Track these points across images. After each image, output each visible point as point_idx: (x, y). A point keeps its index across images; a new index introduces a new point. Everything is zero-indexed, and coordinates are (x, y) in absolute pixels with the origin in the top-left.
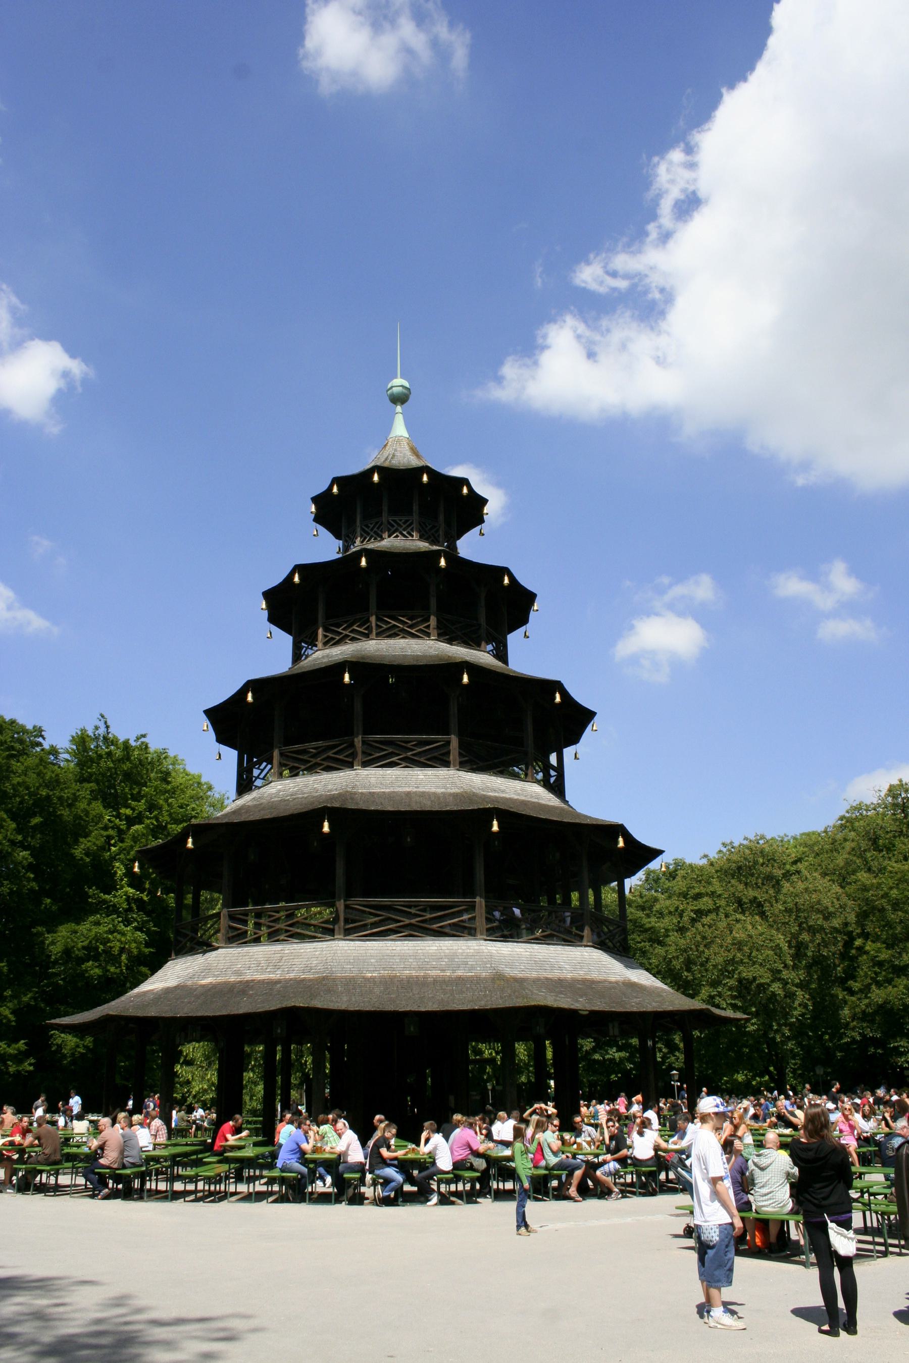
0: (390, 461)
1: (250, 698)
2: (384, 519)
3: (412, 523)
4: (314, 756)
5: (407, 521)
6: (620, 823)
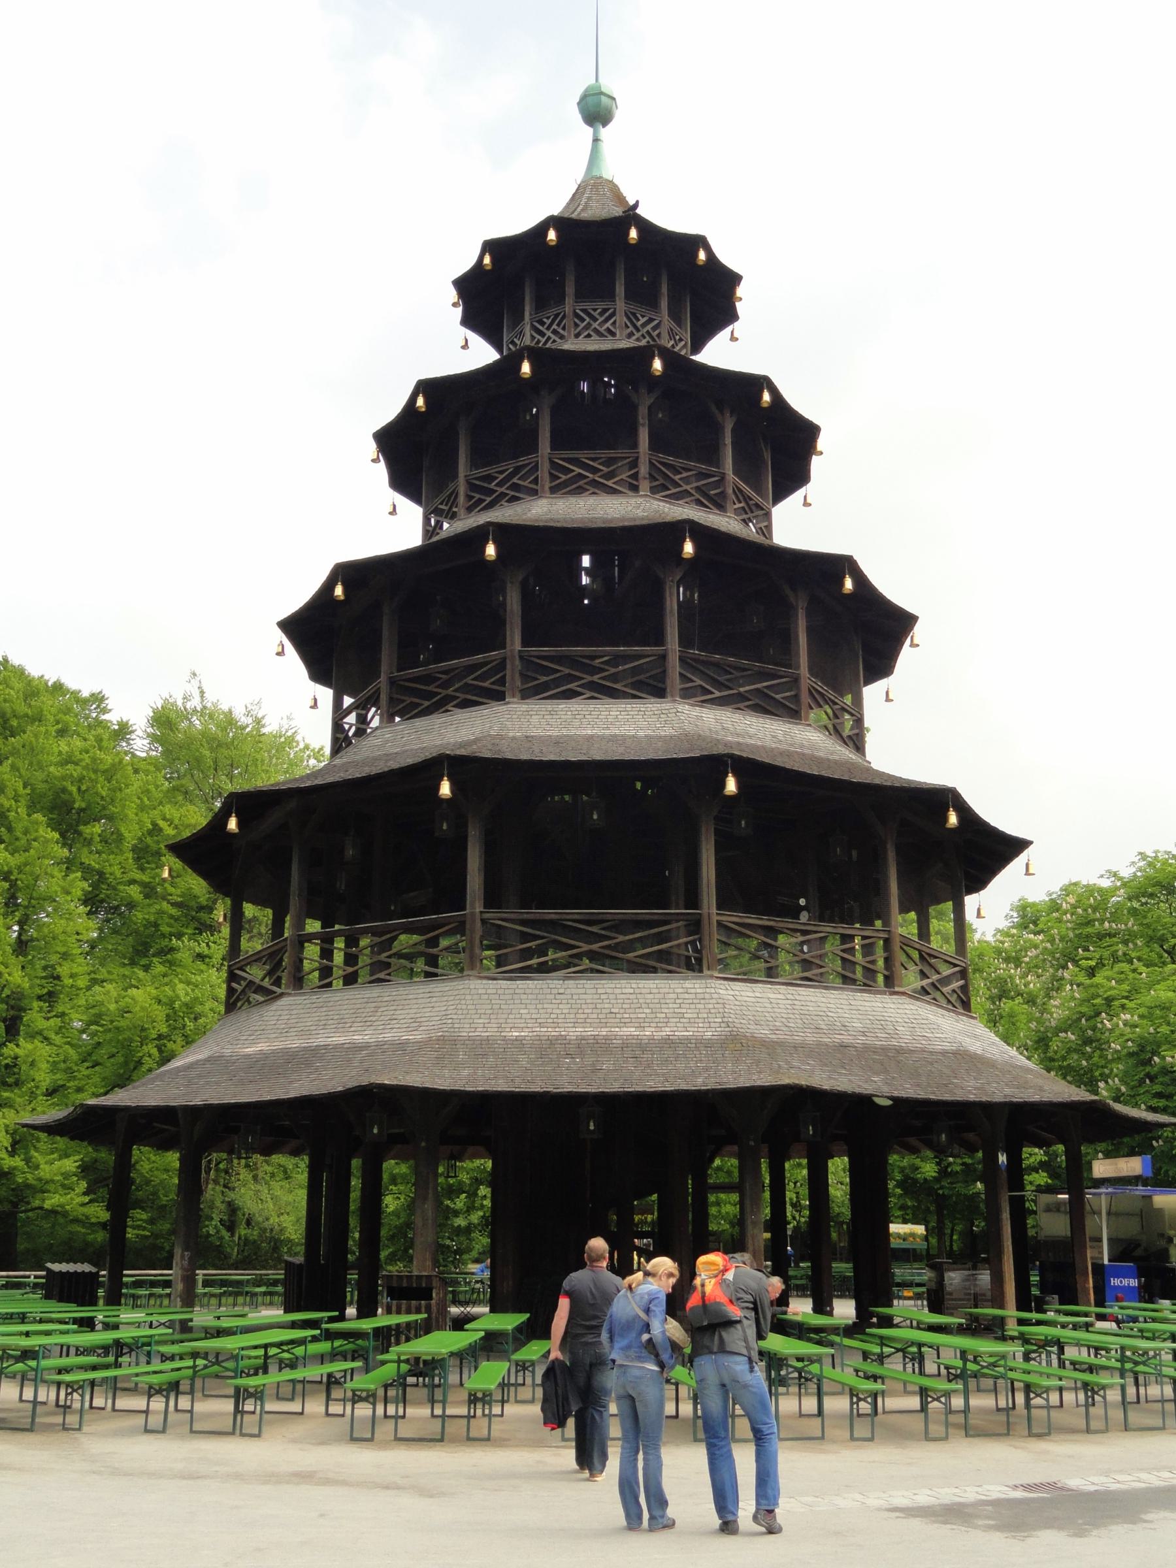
0: (579, 214)
1: (232, 824)
2: (568, 308)
3: (613, 314)
4: (446, 685)
5: (605, 311)
6: (950, 785)
